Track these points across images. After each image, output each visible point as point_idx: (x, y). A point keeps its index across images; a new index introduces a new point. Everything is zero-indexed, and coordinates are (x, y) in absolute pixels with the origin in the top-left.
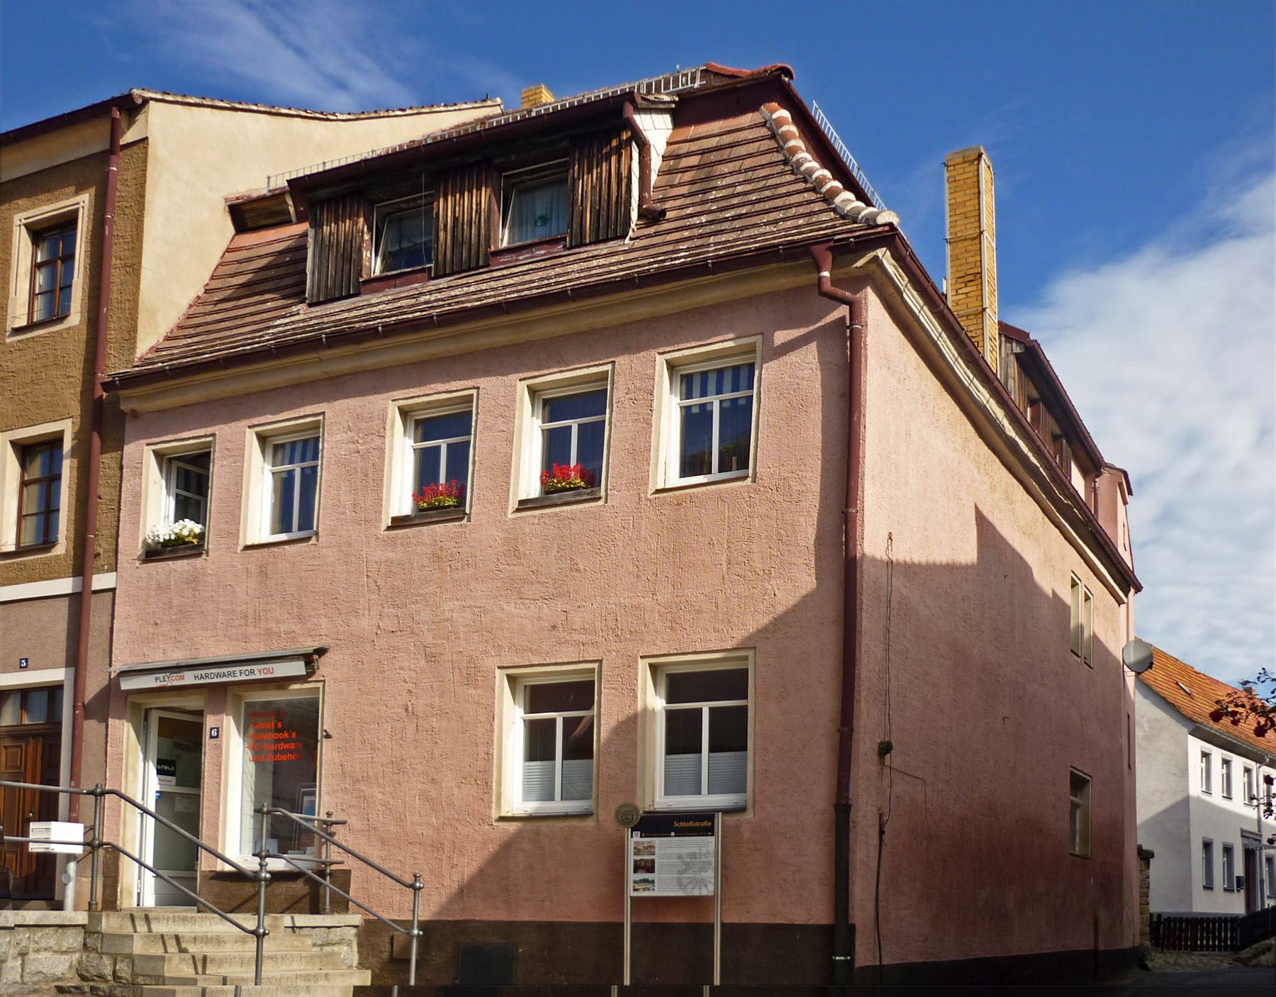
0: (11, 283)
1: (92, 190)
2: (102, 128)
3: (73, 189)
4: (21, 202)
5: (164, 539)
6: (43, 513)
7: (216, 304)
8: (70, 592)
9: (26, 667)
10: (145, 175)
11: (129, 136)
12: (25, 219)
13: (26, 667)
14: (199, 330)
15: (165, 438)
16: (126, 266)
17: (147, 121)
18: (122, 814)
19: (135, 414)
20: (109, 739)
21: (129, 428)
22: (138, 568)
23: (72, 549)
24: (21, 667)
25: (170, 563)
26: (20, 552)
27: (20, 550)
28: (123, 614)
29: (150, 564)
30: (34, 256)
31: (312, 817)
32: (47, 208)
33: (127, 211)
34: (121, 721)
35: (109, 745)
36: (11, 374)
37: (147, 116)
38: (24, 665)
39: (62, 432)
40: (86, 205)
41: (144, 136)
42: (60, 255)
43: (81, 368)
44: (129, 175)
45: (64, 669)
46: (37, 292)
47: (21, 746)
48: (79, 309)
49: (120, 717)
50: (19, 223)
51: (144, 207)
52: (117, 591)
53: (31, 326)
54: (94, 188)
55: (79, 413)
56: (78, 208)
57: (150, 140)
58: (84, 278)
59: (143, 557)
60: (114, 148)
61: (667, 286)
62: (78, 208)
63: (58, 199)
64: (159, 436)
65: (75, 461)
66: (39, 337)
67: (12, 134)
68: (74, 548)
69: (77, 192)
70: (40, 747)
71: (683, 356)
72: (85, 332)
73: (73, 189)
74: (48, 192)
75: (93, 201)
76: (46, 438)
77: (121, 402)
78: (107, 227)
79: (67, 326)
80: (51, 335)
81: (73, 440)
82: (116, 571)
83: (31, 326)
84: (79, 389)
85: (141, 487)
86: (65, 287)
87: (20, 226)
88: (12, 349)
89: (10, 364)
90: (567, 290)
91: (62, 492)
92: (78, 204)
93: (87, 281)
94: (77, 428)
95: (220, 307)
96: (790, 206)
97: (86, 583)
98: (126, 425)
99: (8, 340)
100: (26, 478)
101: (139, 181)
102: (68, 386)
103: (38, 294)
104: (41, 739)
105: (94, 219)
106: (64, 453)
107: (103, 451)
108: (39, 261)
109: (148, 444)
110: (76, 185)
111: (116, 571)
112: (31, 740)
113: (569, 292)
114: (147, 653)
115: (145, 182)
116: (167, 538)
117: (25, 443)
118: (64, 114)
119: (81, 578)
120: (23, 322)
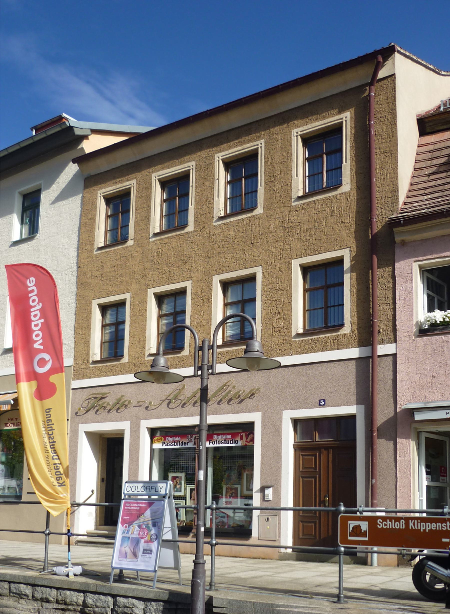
0: (293, 170)
1: (352, 110)
2: (367, 70)
3: (337, 111)
4: (296, 122)
5: (440, 322)
6: (323, 308)
7: (429, 176)
8: (358, 357)
9: (324, 405)
10: (395, 97)
11: (381, 74)
12: (300, 132)
13: (324, 405)
14: (429, 191)
15: (430, 257)
16: (385, 152)
17: (394, 64)
18: (412, 502)
19: (403, 243)
20: (398, 452)
21: (398, 252)
22: (414, 340)
23: (356, 330)
24: (320, 405)
25: (443, 336)
26: (102, 361)
27: (102, 360)
28: (404, 370)
29: (424, 338)
30: (226, 178)
31: (354, 509)
32: (317, 124)
33: (382, 119)
34: (407, 440)
35: (398, 456)
36: (298, 224)
37: (394, 61)
38: (322, 403)
39: (186, 287)
40: (349, 118)
41: (393, 73)
42: (177, 195)
43: (354, 216)
44: (382, 98)
45: (355, 406)
46: (108, 229)
47: (315, 455)
48: (349, 181)
49: (407, 437)
50: (218, 159)
51: (396, 116)
52: (398, 356)
53: (226, 216)
54: (354, 109)
55: (355, 244)
56: (342, 121)
57: (397, 76)
58: (351, 162)
59: (418, 333)
60: (373, 80)
61: (424, 224)
62: (190, 170)
63: (324, 118)
64: (425, 256)
65: (354, 275)
66: (318, 200)
67: (299, 80)
68: (357, 329)
69: (340, 112)
70: (330, 455)
71: (428, 263)
72: (355, 195)
73: (337, 111)
74: (318, 114)
75: (353, 116)
76: (333, 260)
77: (395, 236)
78: (372, 129)
79: (340, 192)
80: (328, 198)
81: (351, 261)
82: (395, 342)
83: (226, 216)
84: (353, 230)
85: (412, 289)
86: (125, 226)
87: (100, 197)
88: (298, 209)
89: (296, 218)
90: (444, 211)
91: (345, 294)
92: (342, 119)
93: (354, 163)
94: (354, 254)
95: (432, 177)
96: (439, 191)
97: (373, 351)
98: (396, 248)
99: (293, 204)
100: (161, 314)
101: (390, 100)
102: (344, 228)
103: (109, 231)
104: (331, 451)
105: (355, 127)
106: (344, 270)
107: (379, 268)
108: (109, 214)
109: (415, 261)
110: (339, 108)
111: (395, 342)
112: (324, 452)
113: (402, 222)
114: (427, 395)
115: (395, 101)
116: (442, 320)
117: (104, 305)
118: (340, 64)
119: (371, 347)
120: (102, 245)
